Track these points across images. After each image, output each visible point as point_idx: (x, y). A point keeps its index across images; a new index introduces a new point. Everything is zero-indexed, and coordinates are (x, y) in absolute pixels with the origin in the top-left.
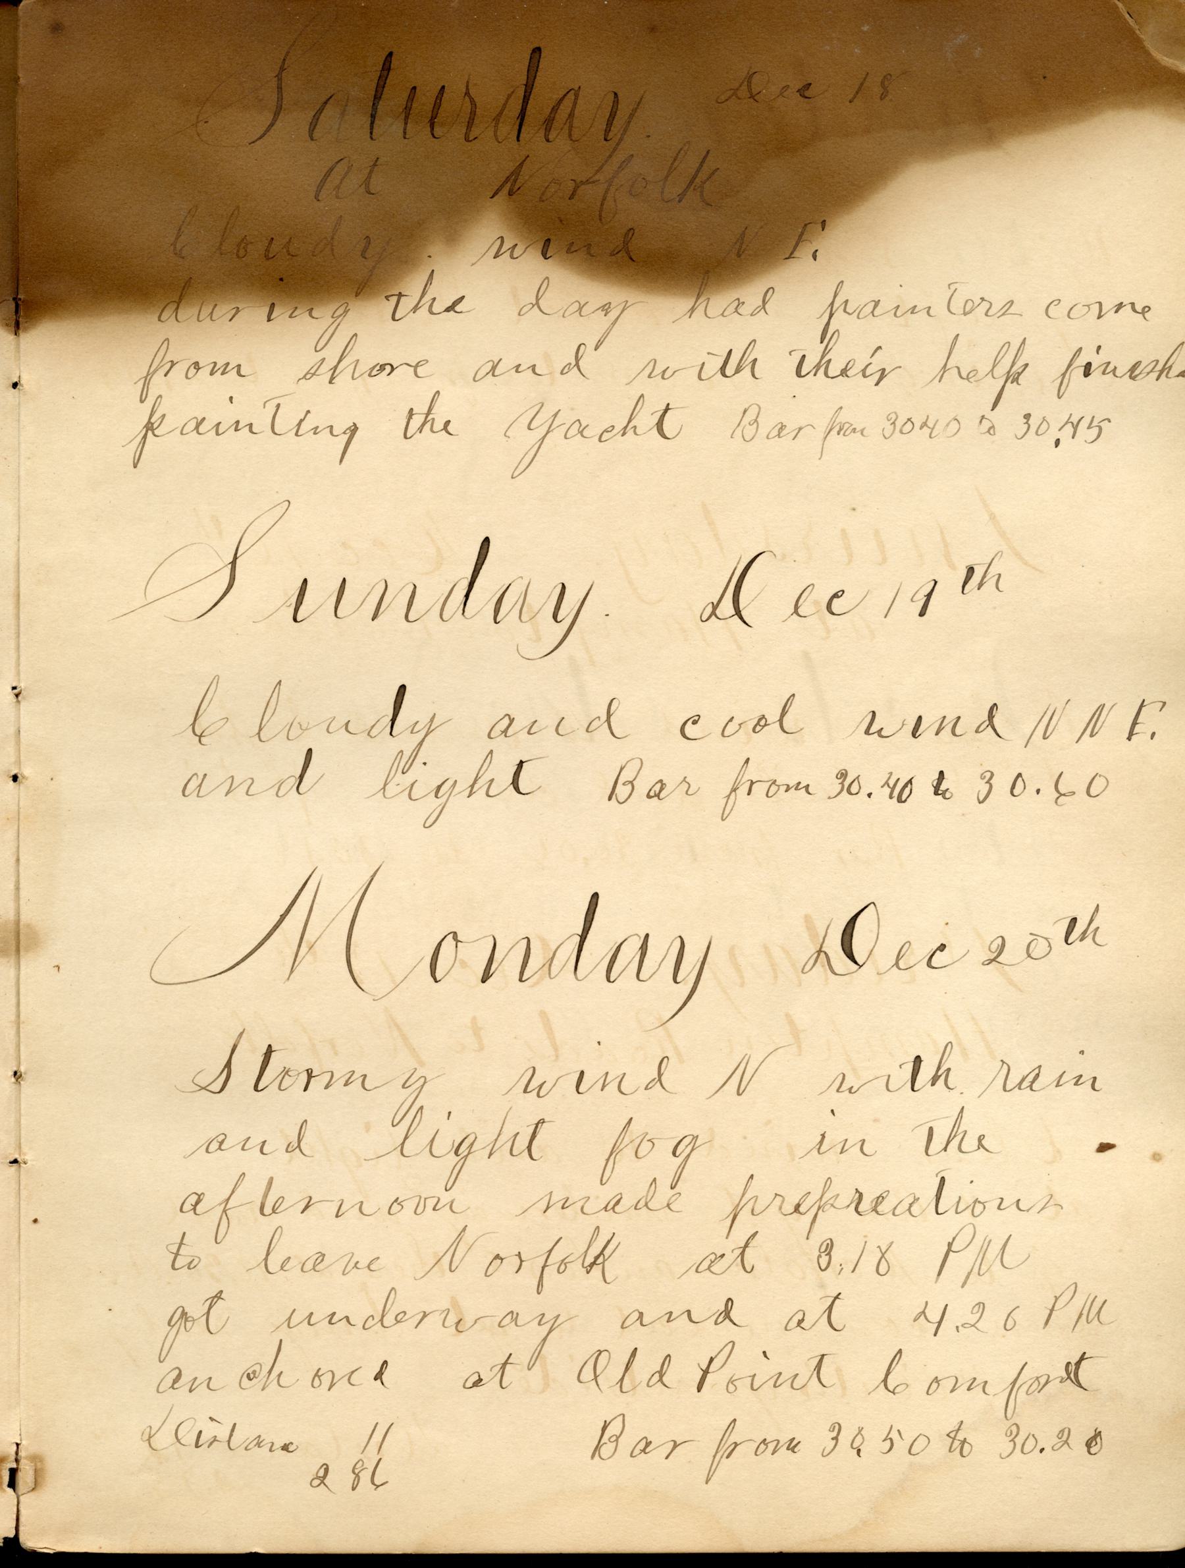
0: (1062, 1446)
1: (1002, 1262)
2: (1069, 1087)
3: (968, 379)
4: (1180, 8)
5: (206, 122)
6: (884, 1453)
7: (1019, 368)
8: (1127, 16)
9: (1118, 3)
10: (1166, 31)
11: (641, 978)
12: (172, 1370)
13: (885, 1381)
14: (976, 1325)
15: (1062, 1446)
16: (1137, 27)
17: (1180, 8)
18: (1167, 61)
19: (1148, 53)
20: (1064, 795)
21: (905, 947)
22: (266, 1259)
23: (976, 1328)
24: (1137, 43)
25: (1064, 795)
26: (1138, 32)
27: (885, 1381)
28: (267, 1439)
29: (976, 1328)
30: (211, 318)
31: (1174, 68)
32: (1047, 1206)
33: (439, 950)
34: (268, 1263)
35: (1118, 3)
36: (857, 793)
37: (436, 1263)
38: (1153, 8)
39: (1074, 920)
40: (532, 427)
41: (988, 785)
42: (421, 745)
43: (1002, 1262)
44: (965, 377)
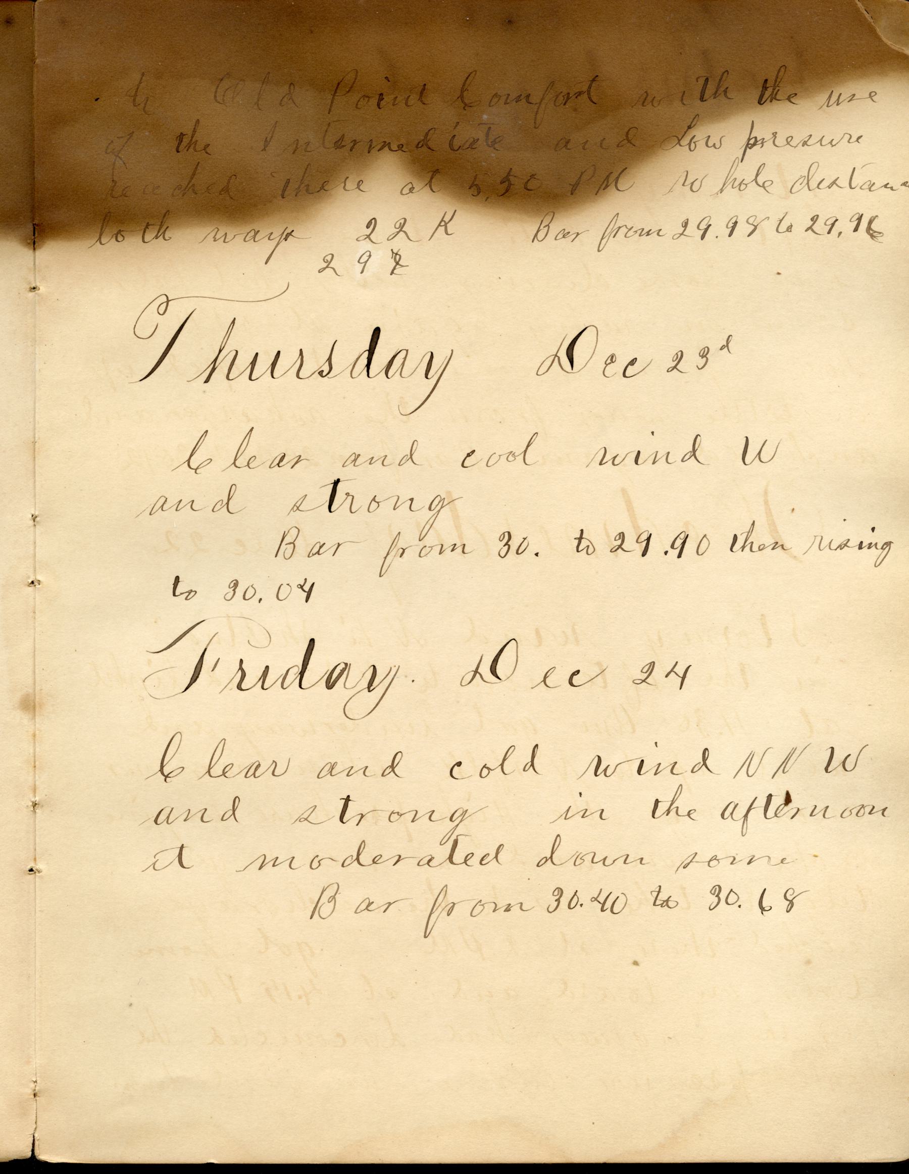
3: (763, 187)
4: (905, 7)
6: (722, 137)
7: (806, 138)
8: (865, 12)
9: (858, 3)
10: (895, 24)
11: (768, 817)
12: (753, 774)
13: (189, 461)
14: (308, 819)
16: (872, 21)
17: (905, 7)
18: (897, 47)
19: (882, 41)
24: (872, 31)
26: (873, 24)
27: (189, 461)
28: (877, 816)
31: (900, 51)
33: (393, 361)
35: (858, 3)
38: (885, 7)
41: (717, 898)
44: (761, 185)
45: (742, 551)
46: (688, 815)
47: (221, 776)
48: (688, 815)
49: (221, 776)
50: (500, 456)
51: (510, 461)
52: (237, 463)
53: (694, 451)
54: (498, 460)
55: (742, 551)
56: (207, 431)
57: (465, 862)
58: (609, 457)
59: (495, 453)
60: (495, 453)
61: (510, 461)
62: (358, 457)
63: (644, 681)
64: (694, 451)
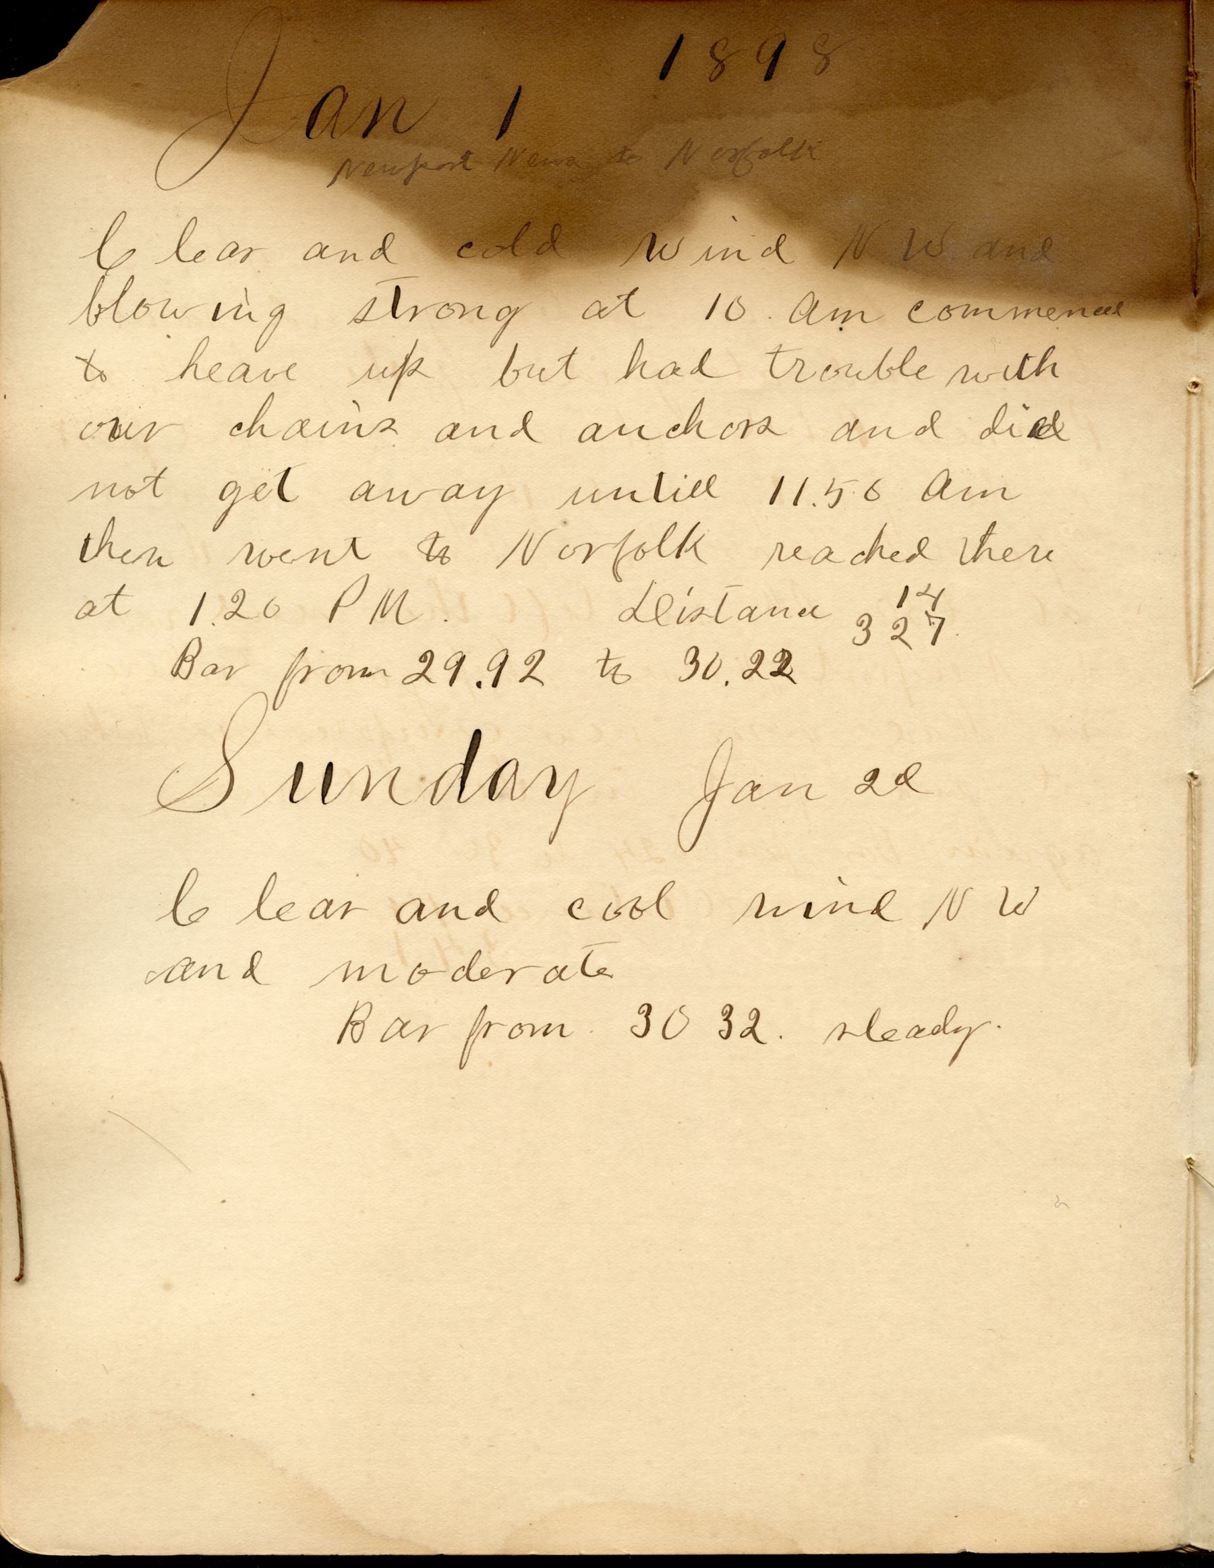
0: (865, 790)
1: (566, 372)
2: (431, 920)
5: (92, 229)
15: (865, 790)
20: (110, 268)
21: (667, 887)
22: (100, 250)
23: (240, 616)
25: (110, 268)
29: (240, 616)
30: (134, 316)
32: (445, 911)
34: (102, 253)
36: (669, 595)
37: (353, 777)
39: (484, 1036)
40: (455, 979)
42: (227, 515)
43: (566, 372)
45: (866, 563)
46: (1003, 558)
47: (1000, 559)
48: (1003, 558)
49: (1000, 559)
50: (272, 557)
51: (1005, 499)
52: (920, 375)
53: (252, 968)
54: (802, 368)
55: (866, 563)
56: (676, 524)
57: (1004, 558)
58: (768, 907)
59: (568, 546)
60: (568, 546)
61: (1005, 499)
62: (325, 248)
63: (235, 613)
64: (252, 968)
